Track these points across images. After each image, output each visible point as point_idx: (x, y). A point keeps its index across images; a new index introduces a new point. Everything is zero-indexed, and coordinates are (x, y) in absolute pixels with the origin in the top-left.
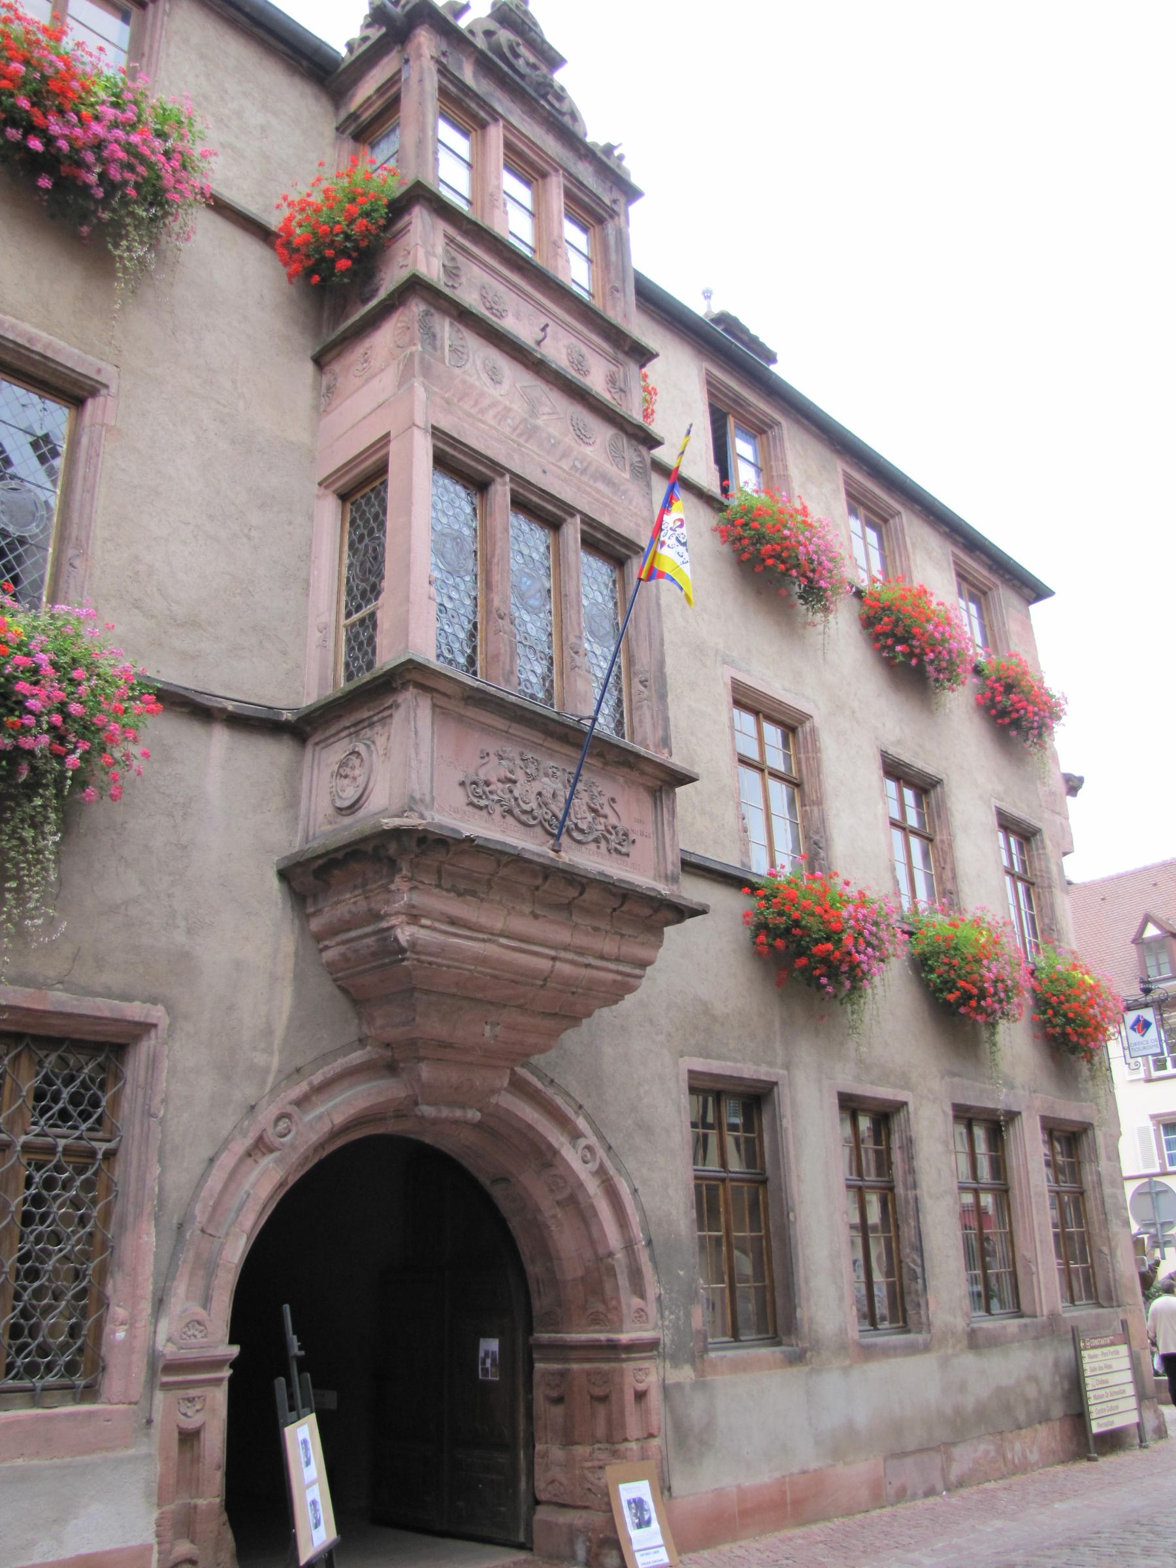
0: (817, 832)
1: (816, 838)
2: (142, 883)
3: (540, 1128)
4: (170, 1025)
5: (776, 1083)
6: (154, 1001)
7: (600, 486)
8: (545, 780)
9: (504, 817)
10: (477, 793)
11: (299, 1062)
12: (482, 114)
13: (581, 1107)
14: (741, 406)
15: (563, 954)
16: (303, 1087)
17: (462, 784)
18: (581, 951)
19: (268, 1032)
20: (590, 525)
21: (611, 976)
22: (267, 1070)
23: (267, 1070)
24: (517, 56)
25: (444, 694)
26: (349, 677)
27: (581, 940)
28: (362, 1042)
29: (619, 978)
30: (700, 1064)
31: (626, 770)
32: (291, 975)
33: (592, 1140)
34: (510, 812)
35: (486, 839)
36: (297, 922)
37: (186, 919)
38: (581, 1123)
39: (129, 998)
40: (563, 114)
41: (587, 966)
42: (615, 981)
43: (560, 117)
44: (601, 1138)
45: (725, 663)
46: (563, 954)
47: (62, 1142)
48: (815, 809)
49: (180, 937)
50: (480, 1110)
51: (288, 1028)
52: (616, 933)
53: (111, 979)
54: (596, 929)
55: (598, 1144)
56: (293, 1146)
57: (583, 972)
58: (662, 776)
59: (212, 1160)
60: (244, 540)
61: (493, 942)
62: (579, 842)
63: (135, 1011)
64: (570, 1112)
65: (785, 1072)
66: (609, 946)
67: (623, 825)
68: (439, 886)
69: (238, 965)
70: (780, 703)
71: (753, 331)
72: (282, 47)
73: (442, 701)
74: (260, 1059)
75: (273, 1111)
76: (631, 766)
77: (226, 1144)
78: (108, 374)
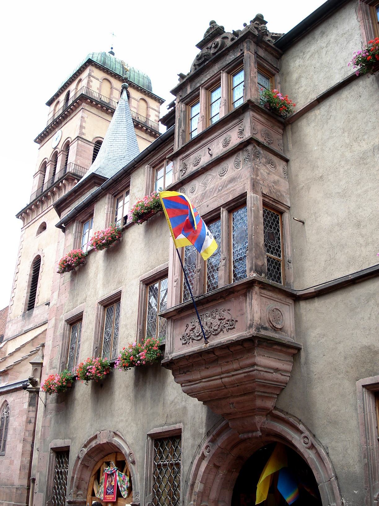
6: (180, 422)
15: (222, 376)
18: (228, 372)
20: (227, 205)
21: (243, 375)
27: (225, 368)
29: (246, 374)
30: (369, 381)
31: (232, 295)
33: (307, 433)
34: (193, 339)
38: (301, 427)
39: (176, 423)
41: (233, 375)
42: (245, 376)
44: (310, 431)
46: (222, 376)
49: (184, 403)
52: (235, 360)
53: (173, 420)
54: (227, 362)
55: (309, 435)
57: (233, 378)
58: (245, 286)
59: (192, 463)
61: (202, 382)
63: (177, 426)
64: (296, 423)
66: (235, 366)
73: (174, 318)
76: (233, 292)
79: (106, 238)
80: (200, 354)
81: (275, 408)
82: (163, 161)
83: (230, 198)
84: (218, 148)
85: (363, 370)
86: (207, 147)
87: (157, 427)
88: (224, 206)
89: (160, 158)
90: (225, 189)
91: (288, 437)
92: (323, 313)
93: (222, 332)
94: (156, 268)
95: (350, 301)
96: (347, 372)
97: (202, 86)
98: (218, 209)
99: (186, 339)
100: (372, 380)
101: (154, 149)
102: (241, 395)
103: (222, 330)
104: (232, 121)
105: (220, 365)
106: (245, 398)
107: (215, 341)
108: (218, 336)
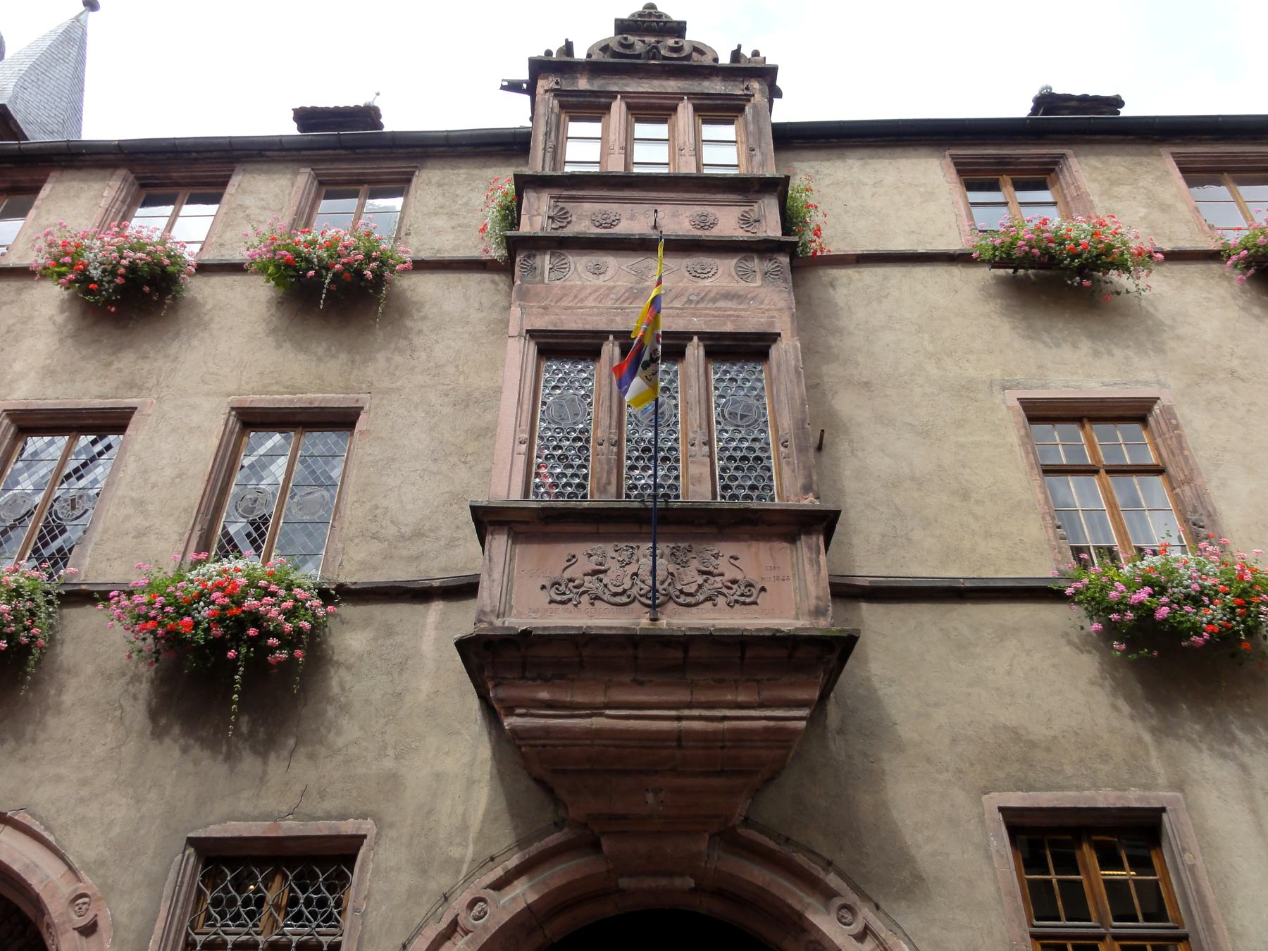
0: (1195, 511)
1: (1194, 518)
2: (361, 728)
3: (774, 890)
4: (377, 834)
5: (1163, 810)
6: (364, 816)
7: (721, 304)
8: (629, 562)
9: (592, 604)
10: (562, 592)
11: (494, 850)
12: (603, 100)
13: (830, 863)
14: (1009, 164)
16: (499, 872)
17: (543, 587)
19: (465, 827)
22: (461, 861)
23: (461, 861)
24: (631, 46)
25: (522, 522)
26: (210, 539)
28: (558, 825)
30: (1016, 800)
32: (488, 777)
34: (597, 598)
35: (544, 628)
36: (494, 732)
37: (395, 748)
38: (833, 880)
39: (343, 817)
40: (688, 57)
41: (724, 718)
43: (691, 63)
45: (1004, 389)
47: (295, 939)
48: (1186, 488)
49: (388, 764)
50: (691, 877)
51: (483, 822)
53: (330, 805)
54: (721, 681)
56: (485, 928)
60: (462, 465)
61: (601, 715)
62: (689, 605)
63: (348, 827)
64: (818, 871)
65: (1179, 795)
67: (752, 576)
68: (524, 678)
69: (438, 776)
70: (1102, 400)
71: (1077, 92)
72: (498, 148)
74: (455, 852)
75: (467, 897)
77: (419, 931)
78: (364, 399)
79: (1085, 256)
80: (630, 641)
81: (747, 822)
82: (362, 183)
83: (729, 328)
84: (678, 219)
85: (1001, 775)
86: (656, 207)
87: (244, 818)
88: (703, 336)
89: (358, 174)
90: (710, 305)
91: (789, 901)
92: (885, 636)
93: (709, 604)
94: (310, 395)
95: (955, 629)
96: (960, 771)
97: (625, 95)
98: (602, 335)
99: (562, 592)
100: (1024, 799)
101: (352, 148)
102: (706, 774)
103: (709, 599)
104: (724, 192)
105: (692, 686)
106: (716, 782)
107: (676, 620)
108: (694, 610)
